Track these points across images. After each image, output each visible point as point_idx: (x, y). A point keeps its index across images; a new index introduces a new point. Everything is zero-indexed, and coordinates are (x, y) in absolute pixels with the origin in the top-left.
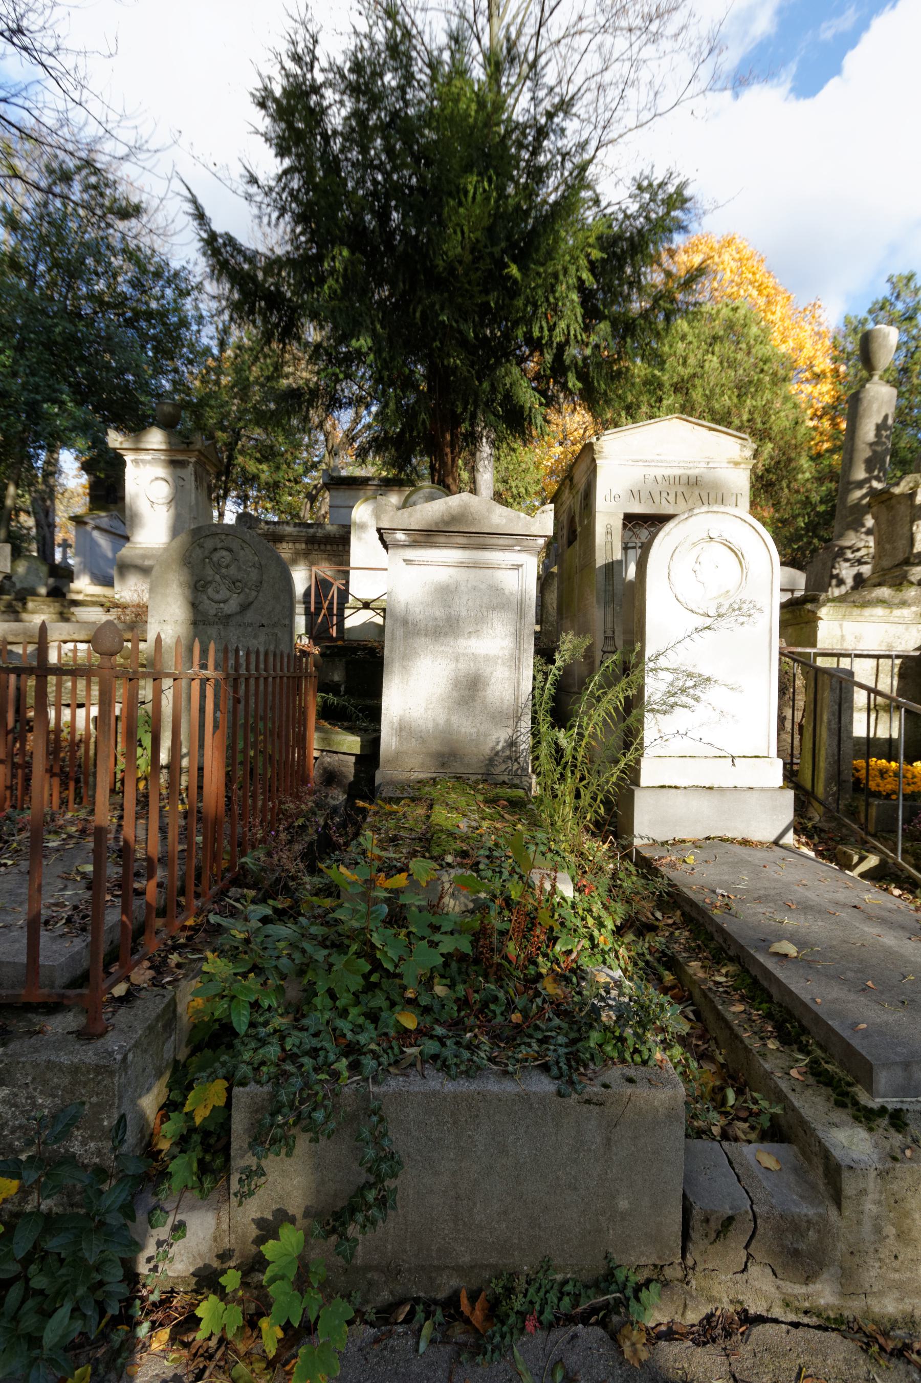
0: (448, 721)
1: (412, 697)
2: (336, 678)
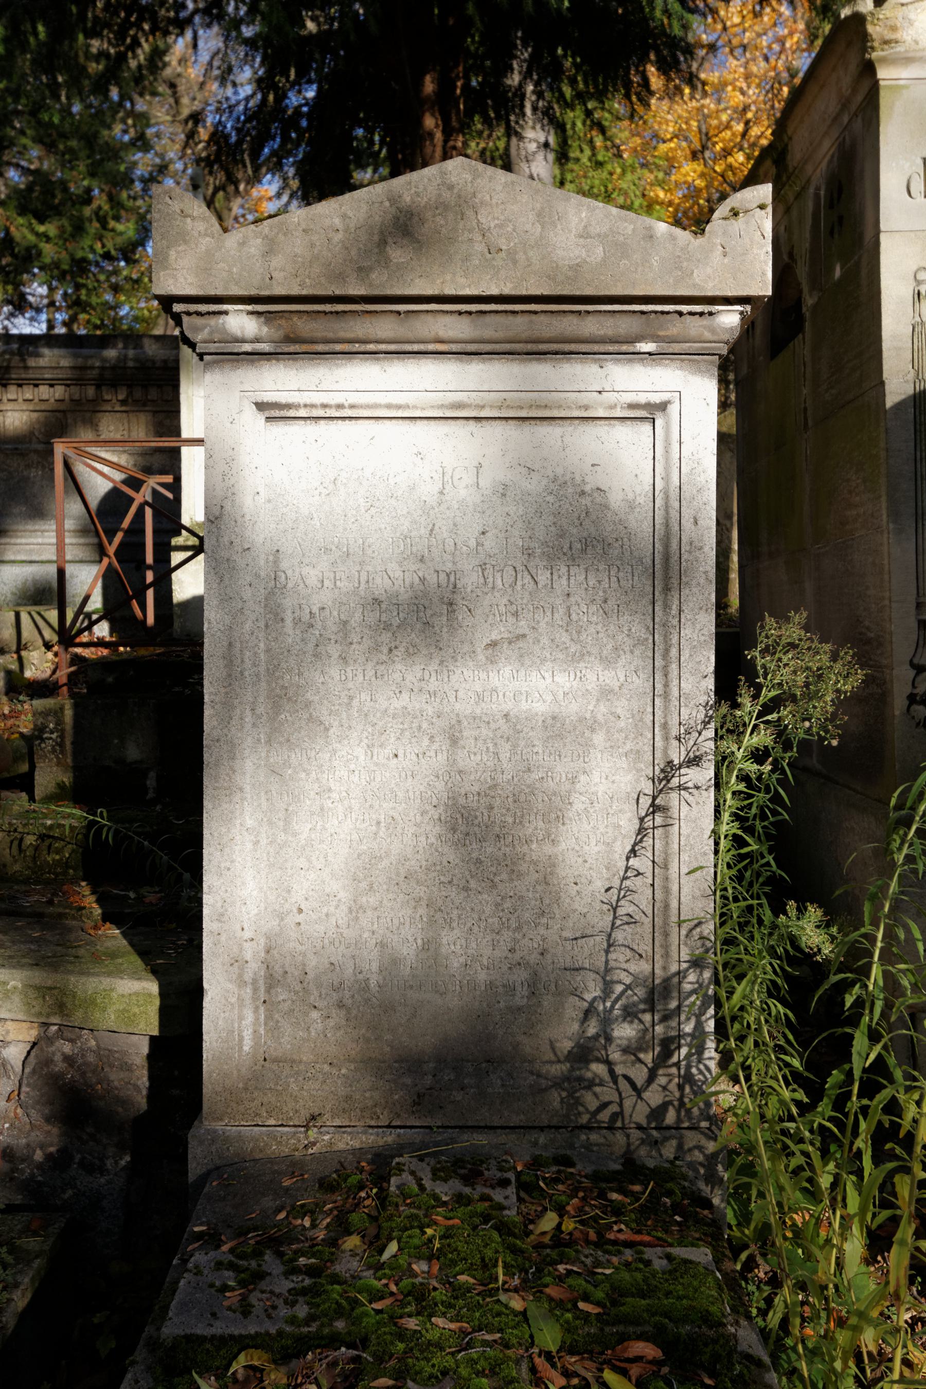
0: (429, 947)
1: (307, 858)
2: (133, 753)
